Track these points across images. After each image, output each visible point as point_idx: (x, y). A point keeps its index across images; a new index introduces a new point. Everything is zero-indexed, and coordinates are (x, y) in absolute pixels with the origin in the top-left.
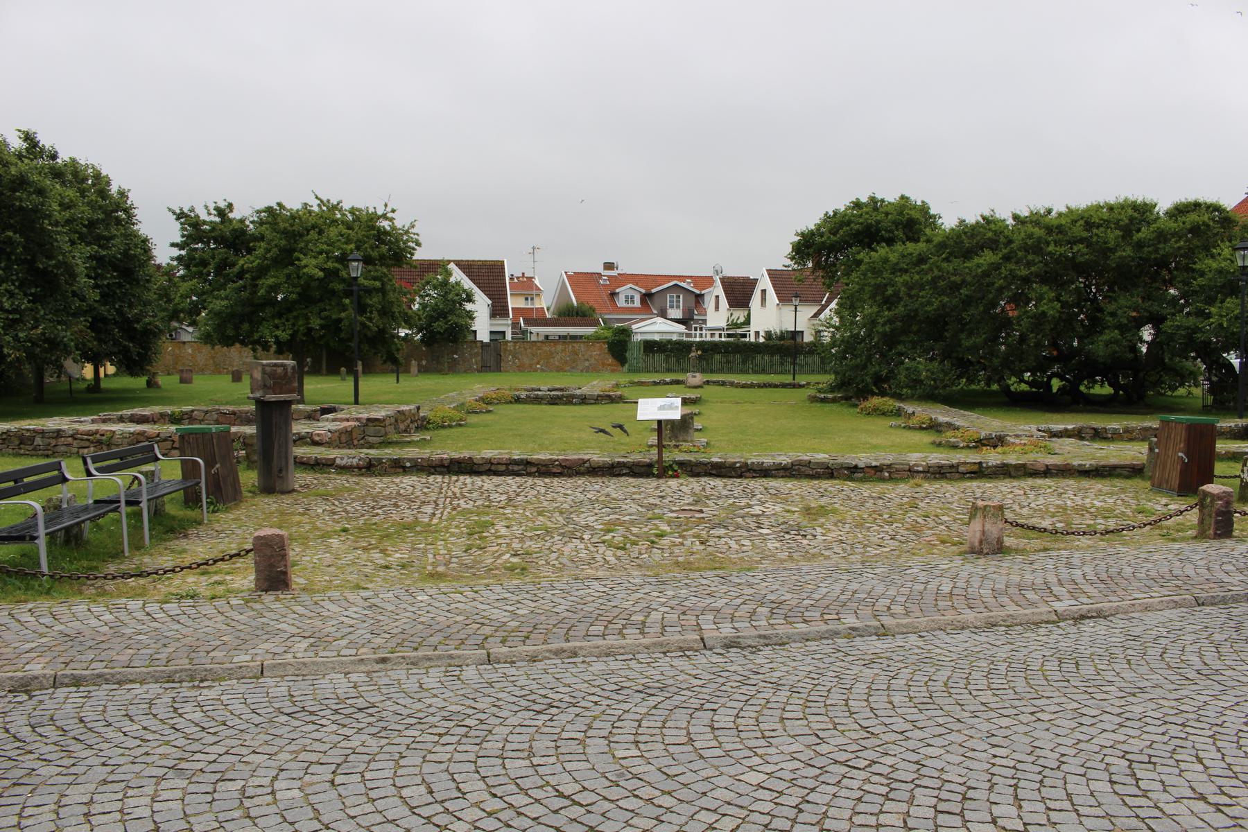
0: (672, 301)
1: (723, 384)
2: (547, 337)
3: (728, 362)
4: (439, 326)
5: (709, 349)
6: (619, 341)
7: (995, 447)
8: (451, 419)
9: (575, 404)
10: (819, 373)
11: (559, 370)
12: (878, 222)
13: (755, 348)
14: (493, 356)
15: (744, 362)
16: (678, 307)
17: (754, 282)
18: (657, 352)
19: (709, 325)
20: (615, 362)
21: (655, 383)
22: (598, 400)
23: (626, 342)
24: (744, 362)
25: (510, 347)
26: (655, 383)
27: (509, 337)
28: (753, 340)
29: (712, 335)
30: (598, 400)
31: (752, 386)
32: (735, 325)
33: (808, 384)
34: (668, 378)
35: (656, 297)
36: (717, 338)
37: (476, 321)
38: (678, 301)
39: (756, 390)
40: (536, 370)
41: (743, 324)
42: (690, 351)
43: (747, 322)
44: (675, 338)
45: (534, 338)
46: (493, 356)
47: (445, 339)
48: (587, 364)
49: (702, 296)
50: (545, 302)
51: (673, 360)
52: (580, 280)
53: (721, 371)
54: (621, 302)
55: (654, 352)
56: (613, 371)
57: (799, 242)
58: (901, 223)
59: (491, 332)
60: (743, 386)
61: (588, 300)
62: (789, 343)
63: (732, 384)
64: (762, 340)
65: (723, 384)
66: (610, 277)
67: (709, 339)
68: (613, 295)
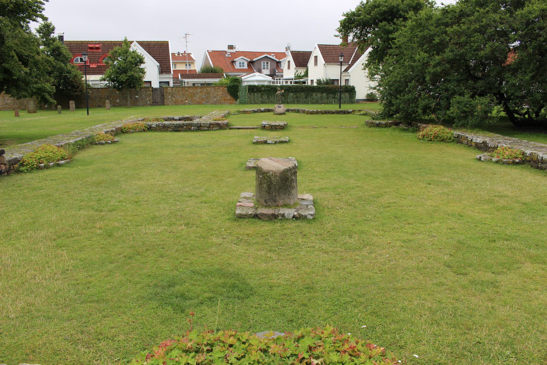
0: (264, 65)
1: (298, 111)
2: (194, 84)
3: (297, 97)
4: (123, 78)
5: (288, 89)
6: (234, 86)
7: (390, 126)
8: (49, 159)
9: (193, 131)
10: (348, 103)
11: (199, 103)
12: (398, 5)
13: (311, 89)
14: (159, 97)
15: (306, 97)
16: (267, 68)
17: (310, 53)
18: (256, 92)
19: (285, 77)
20: (232, 98)
21: (254, 112)
22: (210, 127)
23: (238, 86)
24: (306, 97)
25: (169, 90)
26: (254, 112)
27: (171, 85)
28: (309, 84)
29: (286, 82)
30: (210, 127)
31: (317, 113)
32: (299, 77)
33: (354, 111)
34: (263, 107)
35: (256, 64)
36: (289, 84)
37: (146, 74)
38: (267, 66)
39: (320, 116)
40: (185, 104)
41: (304, 76)
42: (276, 91)
43: (306, 75)
44: (266, 84)
45: (186, 85)
46: (159, 97)
47: (127, 85)
48: (215, 99)
49: (280, 62)
50: (197, 67)
51: (265, 97)
52: (214, 54)
53: (293, 102)
54: (237, 66)
55: (254, 92)
56: (231, 103)
57: (345, 20)
58: (412, 7)
59: (160, 82)
60: (312, 113)
61: (220, 64)
62: (330, 86)
63: (304, 112)
64: (315, 84)
65: (298, 111)
66: (231, 53)
67: (284, 84)
68: (233, 62)
